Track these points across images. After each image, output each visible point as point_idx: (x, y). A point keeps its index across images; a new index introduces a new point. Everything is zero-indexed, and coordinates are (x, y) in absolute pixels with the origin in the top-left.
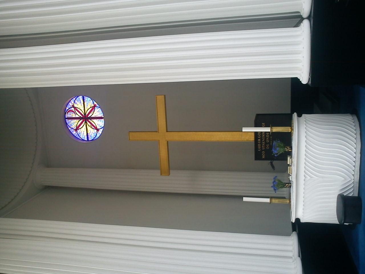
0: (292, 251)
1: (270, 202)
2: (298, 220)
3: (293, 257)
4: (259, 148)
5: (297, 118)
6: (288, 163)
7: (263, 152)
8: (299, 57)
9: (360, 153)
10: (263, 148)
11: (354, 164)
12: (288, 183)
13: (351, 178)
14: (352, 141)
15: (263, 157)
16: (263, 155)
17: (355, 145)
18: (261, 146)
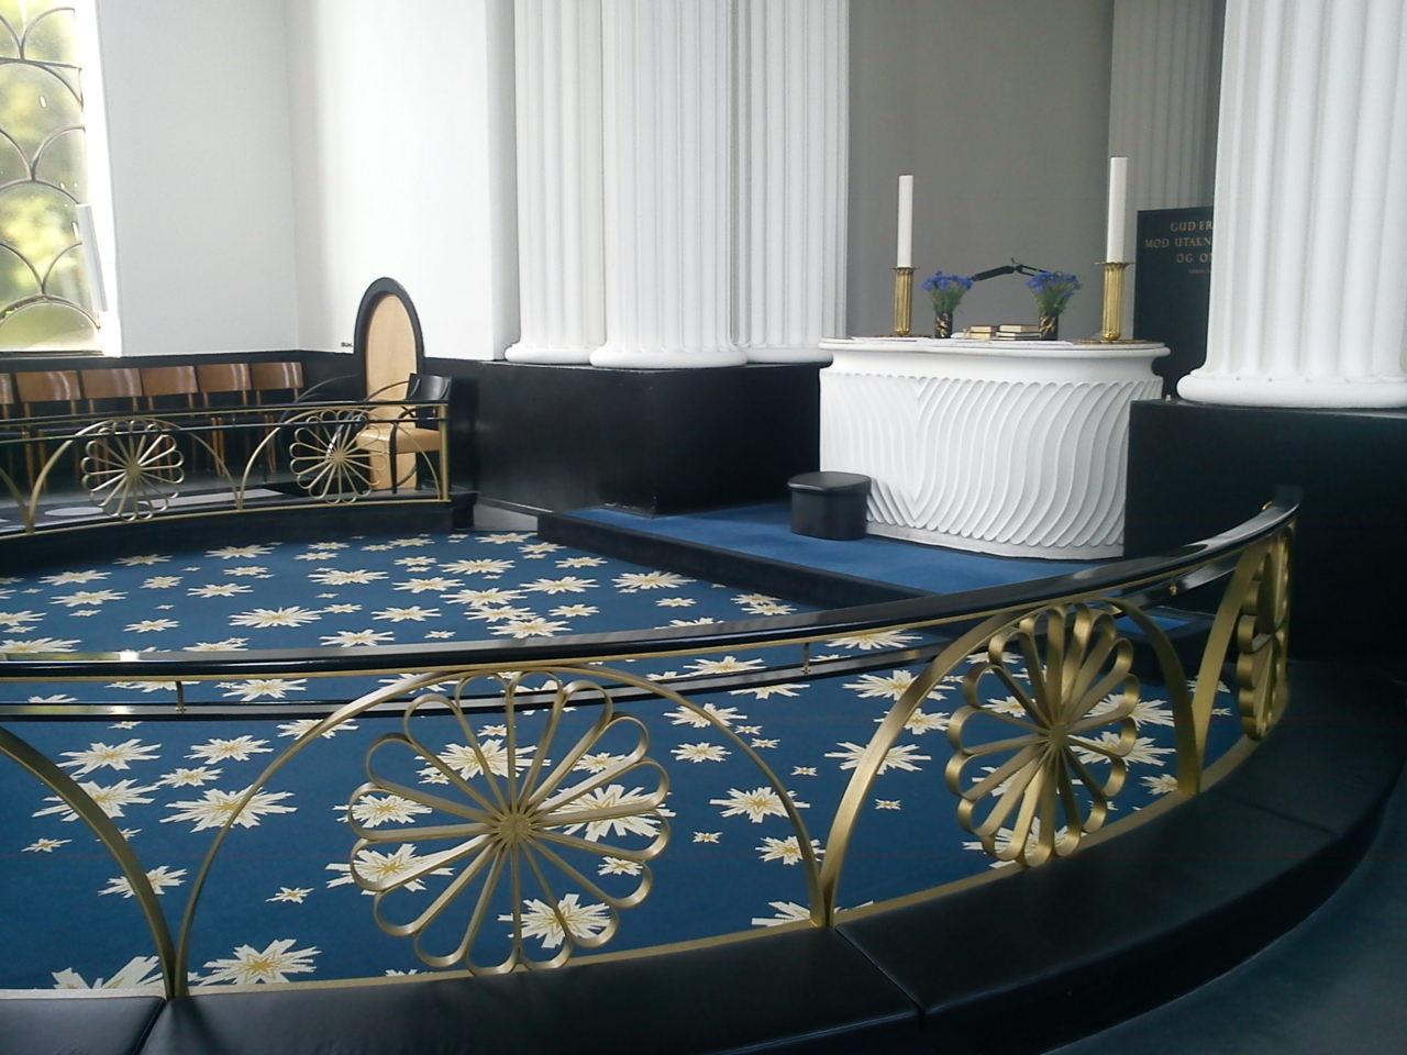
0: (783, 342)
1: (900, 269)
3: (764, 346)
5: (1150, 357)
6: (1003, 328)
7: (1165, 243)
9: (982, 553)
10: (1178, 243)
11: (931, 527)
12: (950, 324)
13: (918, 518)
15: (1149, 244)
17: (1034, 544)
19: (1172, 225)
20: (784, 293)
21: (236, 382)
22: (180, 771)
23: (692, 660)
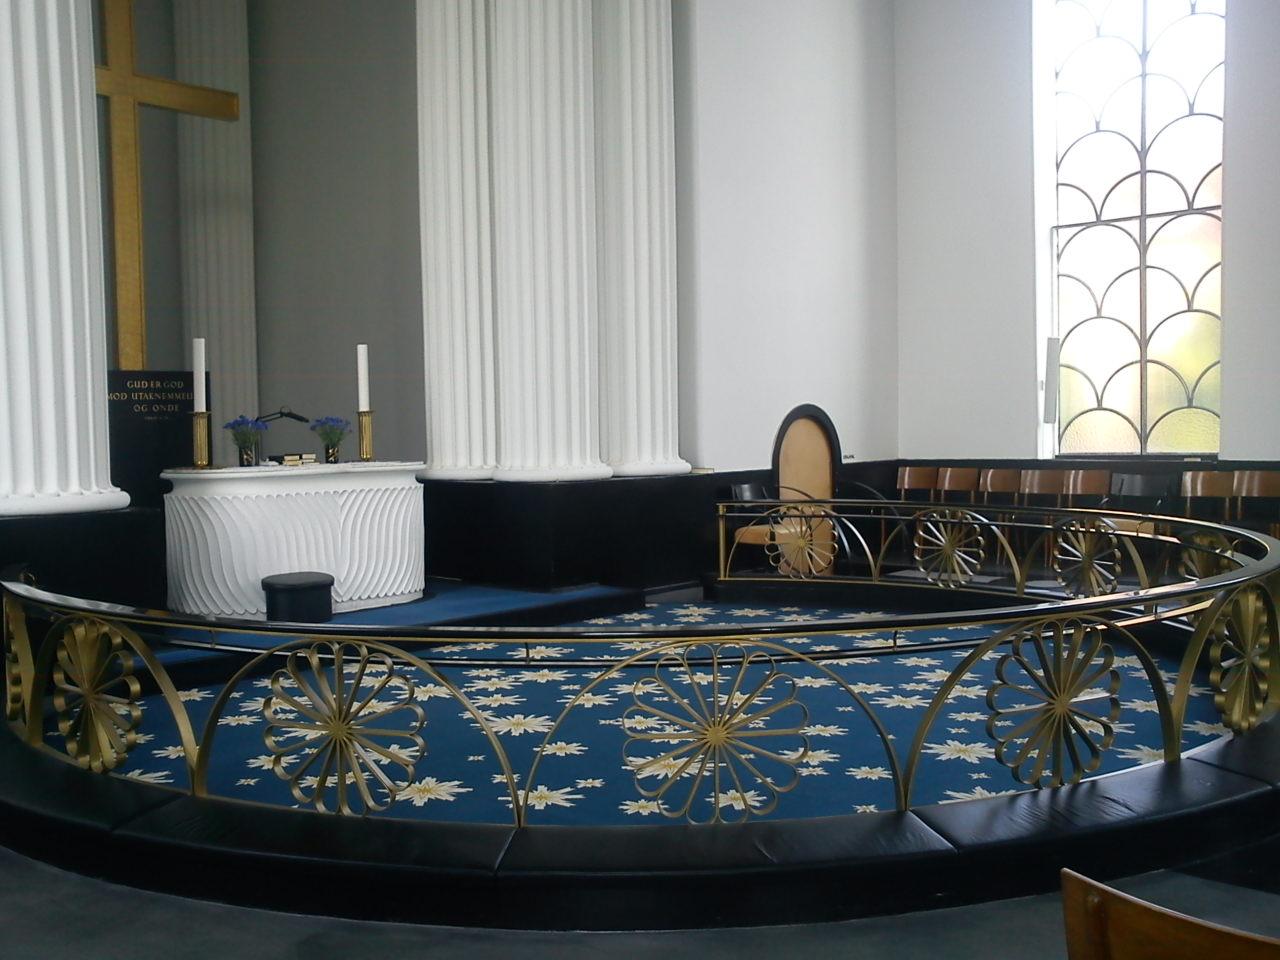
2: (168, 486)
4: (137, 385)
8: (660, 458)
10: (135, 396)
11: (365, 597)
13: (345, 594)
14: (225, 580)
16: (117, 396)
18: (141, 390)
19: (128, 384)
20: (553, 426)
21: (1080, 476)
22: (860, 684)
23: (534, 646)
